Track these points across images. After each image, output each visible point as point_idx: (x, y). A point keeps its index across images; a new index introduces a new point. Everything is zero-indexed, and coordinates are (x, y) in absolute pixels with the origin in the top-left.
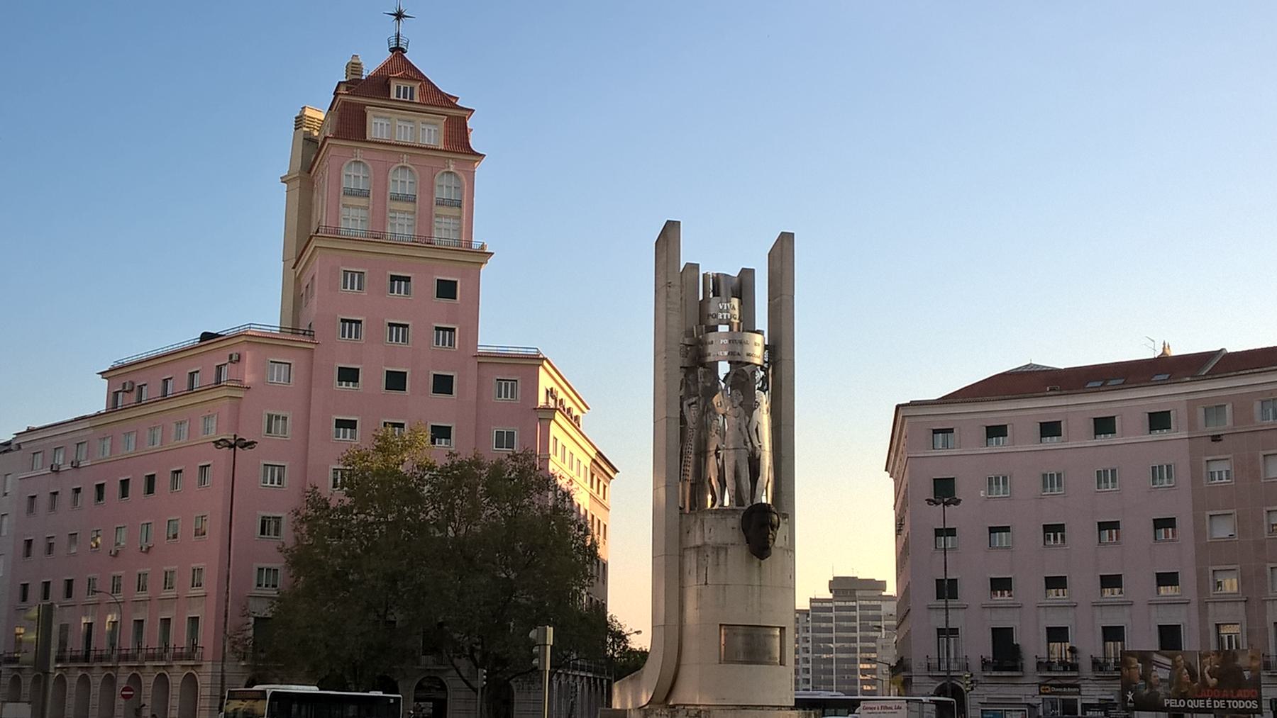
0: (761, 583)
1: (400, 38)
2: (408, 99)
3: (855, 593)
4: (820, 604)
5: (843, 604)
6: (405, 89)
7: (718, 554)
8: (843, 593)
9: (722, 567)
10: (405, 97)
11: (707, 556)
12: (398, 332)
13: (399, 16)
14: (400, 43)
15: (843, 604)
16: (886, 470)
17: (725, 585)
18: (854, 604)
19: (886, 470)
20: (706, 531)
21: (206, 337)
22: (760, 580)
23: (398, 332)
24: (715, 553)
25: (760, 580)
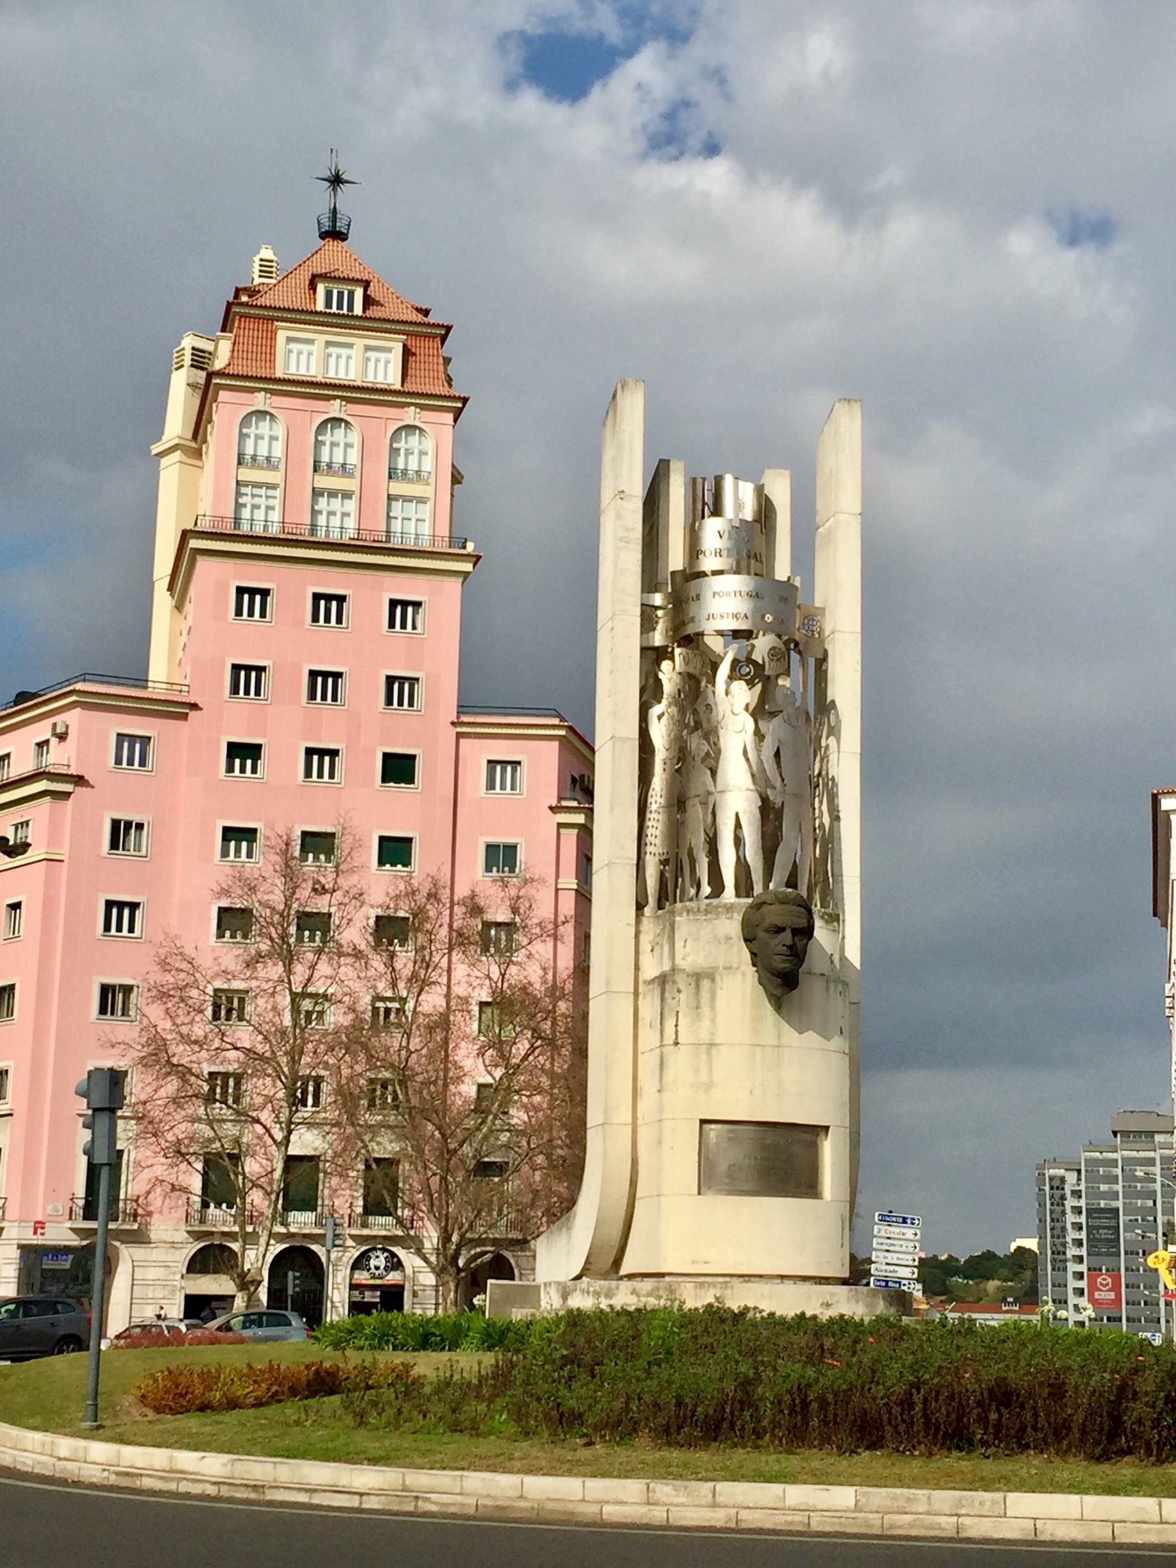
0: (779, 1042)
1: (338, 216)
2: (345, 311)
3: (1153, 1137)
4: (1098, 1154)
5: (1134, 1154)
6: (340, 294)
7: (698, 986)
8: (1134, 1137)
9: (706, 1010)
10: (340, 307)
11: (679, 991)
12: (504, 771)
13: (336, 180)
14: (338, 224)
15: (1134, 1154)
16: (1155, 915)
17: (711, 1044)
18: (1151, 1154)
19: (1155, 915)
20: (679, 945)
21: (22, 697)
22: (779, 1037)
23: (504, 771)
24: (693, 984)
25: (779, 1037)
